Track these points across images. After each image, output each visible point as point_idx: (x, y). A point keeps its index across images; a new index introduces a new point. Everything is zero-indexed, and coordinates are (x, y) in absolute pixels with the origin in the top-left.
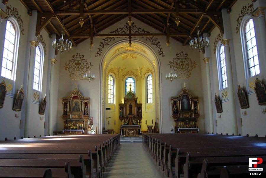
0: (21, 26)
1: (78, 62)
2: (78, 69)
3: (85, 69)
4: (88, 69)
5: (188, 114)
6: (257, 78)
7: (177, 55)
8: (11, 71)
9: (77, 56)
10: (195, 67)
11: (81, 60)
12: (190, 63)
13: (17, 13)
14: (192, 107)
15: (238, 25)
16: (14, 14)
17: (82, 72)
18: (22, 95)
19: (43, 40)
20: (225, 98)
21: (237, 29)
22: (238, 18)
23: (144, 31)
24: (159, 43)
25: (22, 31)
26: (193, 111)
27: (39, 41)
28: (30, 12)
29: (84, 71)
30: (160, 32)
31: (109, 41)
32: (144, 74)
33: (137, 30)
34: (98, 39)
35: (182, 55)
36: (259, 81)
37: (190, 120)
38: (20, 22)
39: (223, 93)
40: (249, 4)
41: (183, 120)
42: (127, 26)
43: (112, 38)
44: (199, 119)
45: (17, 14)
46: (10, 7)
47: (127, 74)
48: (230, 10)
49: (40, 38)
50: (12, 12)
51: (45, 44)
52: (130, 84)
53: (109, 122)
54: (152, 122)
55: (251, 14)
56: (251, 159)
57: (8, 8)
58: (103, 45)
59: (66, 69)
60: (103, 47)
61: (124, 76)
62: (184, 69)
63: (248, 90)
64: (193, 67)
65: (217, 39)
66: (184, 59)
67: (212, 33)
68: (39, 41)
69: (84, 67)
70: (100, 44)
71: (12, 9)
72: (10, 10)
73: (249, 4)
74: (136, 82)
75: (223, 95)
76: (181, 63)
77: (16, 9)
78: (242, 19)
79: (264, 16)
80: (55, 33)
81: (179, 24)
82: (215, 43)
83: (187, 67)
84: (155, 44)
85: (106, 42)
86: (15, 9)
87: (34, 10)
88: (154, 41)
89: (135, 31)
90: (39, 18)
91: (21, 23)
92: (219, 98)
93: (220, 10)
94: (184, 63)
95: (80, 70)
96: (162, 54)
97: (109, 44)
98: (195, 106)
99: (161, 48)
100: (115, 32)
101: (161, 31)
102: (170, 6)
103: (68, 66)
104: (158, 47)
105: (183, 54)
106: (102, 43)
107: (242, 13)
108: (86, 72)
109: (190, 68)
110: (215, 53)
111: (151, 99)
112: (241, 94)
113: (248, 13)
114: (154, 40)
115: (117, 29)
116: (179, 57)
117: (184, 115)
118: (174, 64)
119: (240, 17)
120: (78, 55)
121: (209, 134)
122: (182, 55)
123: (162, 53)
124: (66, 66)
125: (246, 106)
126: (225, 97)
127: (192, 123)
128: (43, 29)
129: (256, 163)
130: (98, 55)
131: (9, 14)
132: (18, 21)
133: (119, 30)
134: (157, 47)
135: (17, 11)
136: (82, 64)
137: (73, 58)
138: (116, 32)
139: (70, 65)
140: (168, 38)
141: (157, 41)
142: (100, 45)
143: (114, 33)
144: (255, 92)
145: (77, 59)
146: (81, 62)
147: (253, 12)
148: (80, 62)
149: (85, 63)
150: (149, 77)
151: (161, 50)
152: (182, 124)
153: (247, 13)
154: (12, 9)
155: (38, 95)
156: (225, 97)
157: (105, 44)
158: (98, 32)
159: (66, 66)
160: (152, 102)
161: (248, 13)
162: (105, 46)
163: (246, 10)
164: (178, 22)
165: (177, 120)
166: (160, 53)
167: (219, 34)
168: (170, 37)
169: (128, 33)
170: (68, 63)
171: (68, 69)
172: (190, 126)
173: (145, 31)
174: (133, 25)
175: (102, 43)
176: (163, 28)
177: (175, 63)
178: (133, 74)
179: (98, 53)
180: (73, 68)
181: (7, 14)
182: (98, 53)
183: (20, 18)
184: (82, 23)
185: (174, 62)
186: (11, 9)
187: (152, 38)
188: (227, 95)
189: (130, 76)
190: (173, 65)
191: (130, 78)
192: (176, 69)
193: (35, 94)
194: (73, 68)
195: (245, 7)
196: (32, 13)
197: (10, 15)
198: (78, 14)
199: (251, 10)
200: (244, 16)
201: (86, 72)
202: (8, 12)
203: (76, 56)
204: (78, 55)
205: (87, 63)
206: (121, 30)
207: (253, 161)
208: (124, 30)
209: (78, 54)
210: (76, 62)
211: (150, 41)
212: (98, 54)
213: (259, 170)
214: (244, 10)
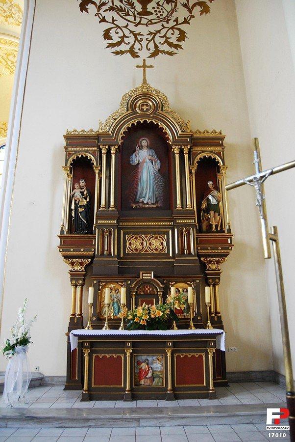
5: (158, 232)
10: (205, 10)
14: (186, 195)
26: (188, 214)
37: (169, 272)
41: (124, 269)
44: (228, 269)
56: (270, 411)
62: (154, 16)
64: (197, 10)
98: (202, 193)
117: (135, 244)
125: (69, 154)
127: (183, 294)
129: (278, 417)
152: (115, 295)
165: (87, 274)
172: (156, 311)
207: (274, 414)
213: (283, 429)
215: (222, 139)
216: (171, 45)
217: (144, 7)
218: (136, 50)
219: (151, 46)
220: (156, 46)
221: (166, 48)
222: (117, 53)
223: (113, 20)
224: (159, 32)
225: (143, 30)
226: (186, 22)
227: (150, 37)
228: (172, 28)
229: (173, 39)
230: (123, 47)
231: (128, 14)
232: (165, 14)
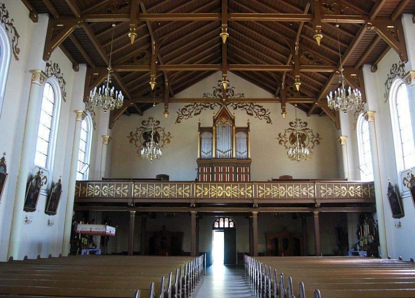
0: (63, 89)
8: (83, 174)
13: (58, 71)
15: (387, 91)
21: (385, 97)
22: (387, 81)
25: (14, 53)
38: (62, 83)
45: (59, 73)
49: (54, 70)
51: (64, 82)
57: (48, 65)
68: (52, 74)
71: (52, 66)
75: (406, 182)
77: (57, 64)
82: (355, 114)
86: (56, 65)
87: (82, 63)
90: (89, 73)
91: (14, 38)
93: (361, 67)
101: (273, 92)
107: (392, 73)
128: (58, 48)
132: (59, 82)
140: (283, 105)
144: (410, 195)
183: (62, 78)
195: (395, 66)
196: (37, 16)
202: (48, 71)
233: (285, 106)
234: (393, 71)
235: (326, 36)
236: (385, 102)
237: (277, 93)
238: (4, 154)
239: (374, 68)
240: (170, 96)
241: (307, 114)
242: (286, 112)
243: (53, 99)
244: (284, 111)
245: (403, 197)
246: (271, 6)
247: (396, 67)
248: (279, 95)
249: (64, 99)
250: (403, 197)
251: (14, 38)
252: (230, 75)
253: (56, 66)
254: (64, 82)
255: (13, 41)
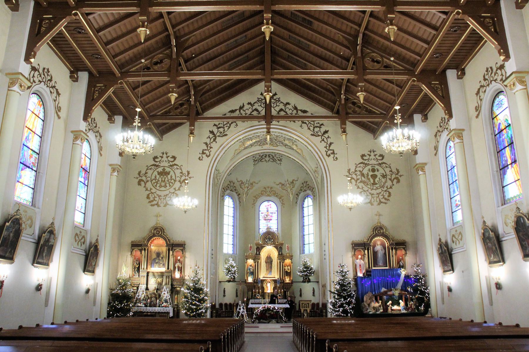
1: (164, 170)
2: (163, 184)
3: (177, 185)
4: (183, 184)
6: (518, 208)
7: (363, 156)
9: (162, 157)
11: (171, 166)
12: (388, 173)
13: (49, 78)
15: (479, 102)
16: (44, 80)
17: (172, 190)
18: (52, 236)
19: (96, 127)
20: (458, 246)
21: (477, 110)
22: (479, 89)
23: (296, 108)
24: (326, 132)
27: (89, 130)
28: (74, 78)
29: (175, 189)
30: (329, 114)
31: (226, 129)
32: (297, 194)
33: (282, 106)
34: (204, 127)
35: (372, 157)
36: (521, 213)
38: (55, 94)
39: (453, 236)
40: (497, 63)
42: (262, 100)
43: (232, 123)
45: (50, 80)
46: (37, 67)
47: (262, 194)
48: (464, 73)
50: (41, 76)
52: (269, 216)
53: (224, 291)
54: (314, 293)
55: (501, 82)
57: (34, 69)
58: (214, 136)
59: (139, 184)
60: (214, 140)
61: (257, 198)
63: (501, 231)
65: (441, 126)
66: (377, 165)
67: (467, 70)
68: (89, 130)
69: (175, 181)
70: (208, 134)
71: (41, 71)
72: (37, 73)
73: (497, 63)
74: (279, 210)
75: (454, 239)
76: (371, 173)
77: (48, 70)
78: (485, 91)
79: (463, 142)
80: (120, 113)
81: (365, 99)
83: (383, 180)
84: (319, 136)
85: (221, 130)
86: (46, 70)
88: (317, 129)
89: (278, 109)
91: (56, 97)
92: (446, 245)
93: (444, 72)
94: (376, 173)
95: (168, 185)
96: (332, 156)
97: (226, 135)
99: (331, 144)
100: (238, 111)
101: (331, 109)
102: (347, 63)
103: (144, 178)
104: (325, 140)
105: (375, 155)
106: (212, 132)
107: (485, 79)
108: (179, 189)
109: (389, 183)
110: (436, 153)
111: (312, 246)
112: (489, 238)
113: (496, 80)
114: (317, 127)
115: (244, 106)
116: (366, 162)
118: (356, 175)
119: (481, 86)
120: (165, 156)
121: (433, 320)
122: (372, 157)
123: (332, 153)
124: (141, 178)
125: (302, 304)
126: (457, 242)
128: (99, 106)
130: (204, 156)
131: (34, 81)
132: (51, 92)
133: (247, 107)
134: (323, 140)
135: (49, 74)
136: (172, 173)
137: (153, 163)
138: (240, 111)
139: (149, 175)
140: (343, 123)
141: (323, 129)
142: (209, 137)
143: (237, 114)
144: (514, 236)
145: (162, 164)
146: (170, 170)
147: (507, 78)
148: (167, 170)
149: (178, 172)
150: (306, 200)
151: (330, 146)
153: (495, 80)
154: (41, 71)
155: (84, 237)
156: (457, 242)
157: (218, 134)
158: (204, 110)
159: (141, 178)
160: (312, 251)
161: (496, 80)
162: (217, 138)
163: (493, 75)
164: (361, 96)
166: (329, 152)
167: (444, 118)
168: (347, 122)
169: (263, 113)
170: (143, 172)
171: (142, 183)
173: (298, 108)
174: (275, 97)
175: (212, 132)
176: (335, 104)
177: (358, 173)
178: (274, 194)
179: (203, 153)
180: (154, 181)
181: (32, 81)
182: (203, 153)
183: (54, 87)
184: (173, 97)
185: (356, 171)
186: (39, 72)
187: (312, 123)
188: (461, 239)
189: (268, 198)
190: (354, 176)
191: (268, 201)
192: (361, 185)
193: (77, 234)
194: (154, 181)
195: (490, 69)
197: (37, 83)
198: (166, 79)
199: (502, 75)
200: (488, 85)
201: (179, 189)
202: (33, 76)
203: (160, 158)
204: (165, 156)
205: (181, 173)
206: (250, 106)
208: (256, 106)
209: (163, 154)
210: (160, 169)
211: (309, 129)
212: (205, 153)
214: (488, 74)
215: (185, 245)
216: (386, 199)
217: (374, 181)
218: (159, 203)
219: (378, 200)
220: (380, 200)
221: (383, 200)
222: (152, 205)
223: (362, 188)
224: (380, 193)
225: (374, 192)
226: (391, 188)
227: (377, 196)
228: (386, 191)
229: (386, 197)
230: (155, 202)
231: (368, 185)
232: (382, 184)
233: (345, 124)
234: (441, 125)
235: (369, 95)
236: (435, 155)
237: (335, 110)
238: (98, 236)
239: (425, 118)
240: (198, 114)
241: (374, 136)
242: (347, 132)
243: (90, 154)
244: (344, 132)
245: (503, 239)
246: (314, 65)
247: (492, 70)
248: (338, 112)
249: (58, 115)
250: (503, 239)
251: (56, 97)
252: (275, 87)
253: (47, 71)
254: (58, 94)
255: (55, 101)
